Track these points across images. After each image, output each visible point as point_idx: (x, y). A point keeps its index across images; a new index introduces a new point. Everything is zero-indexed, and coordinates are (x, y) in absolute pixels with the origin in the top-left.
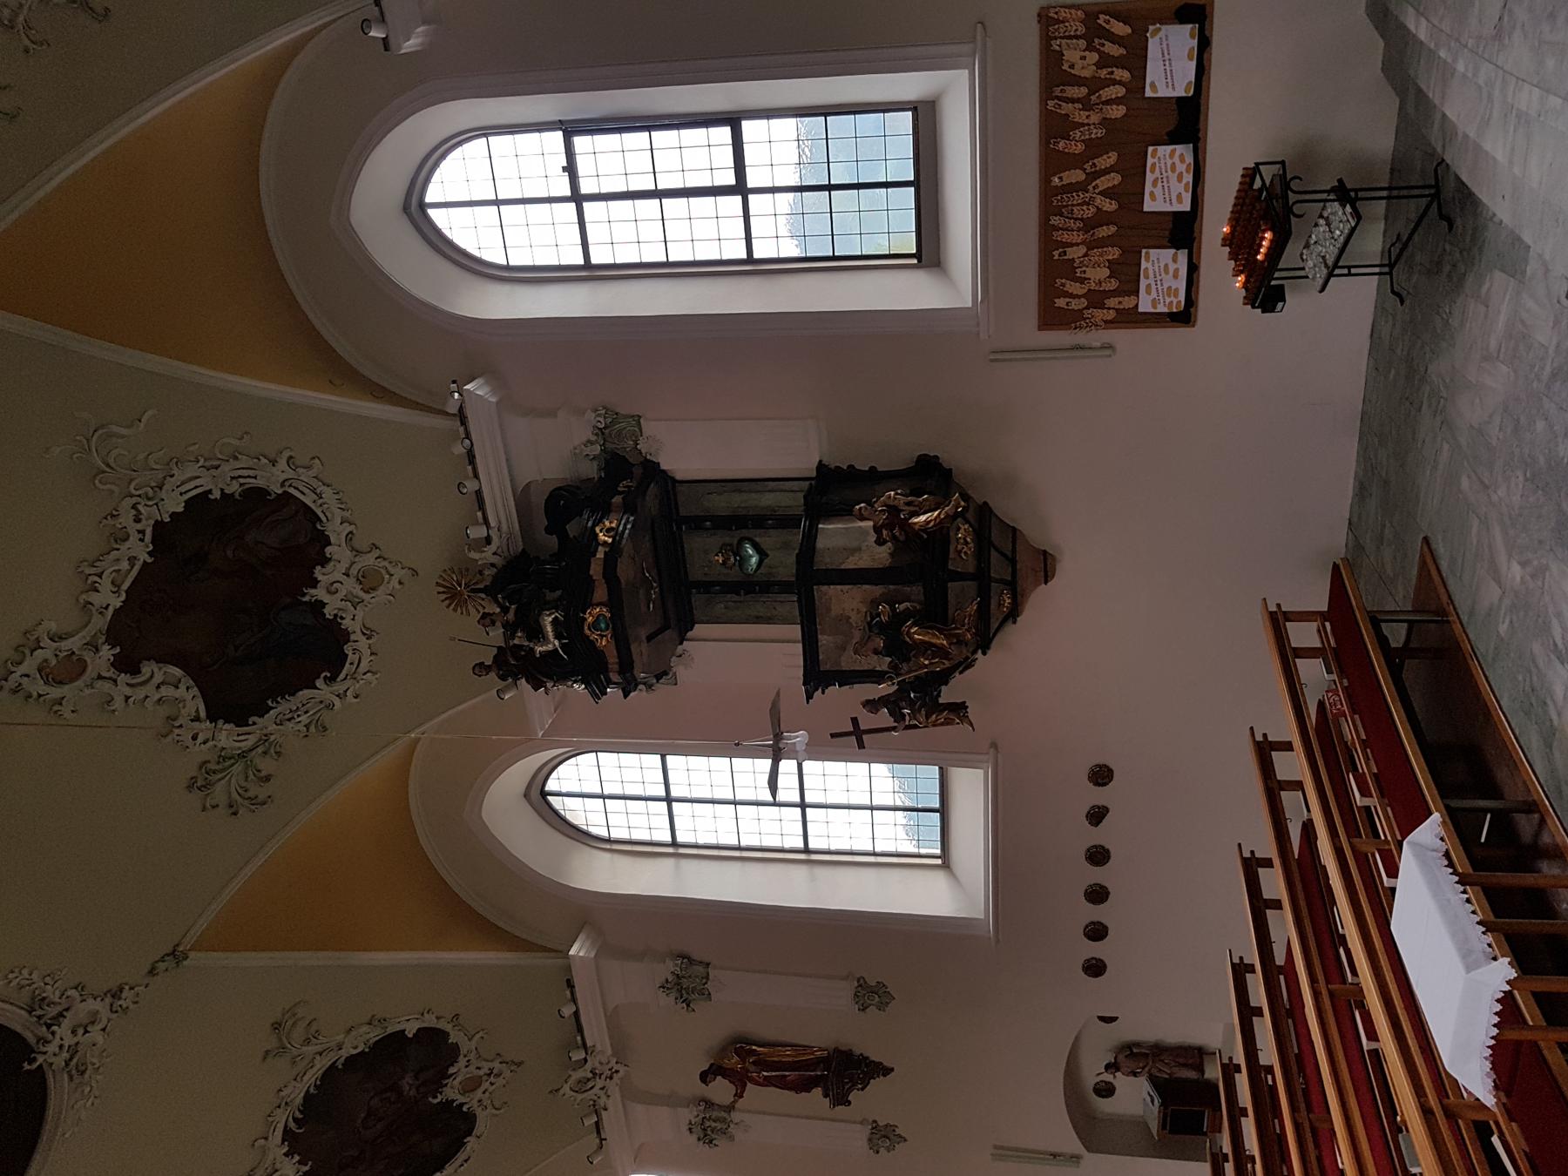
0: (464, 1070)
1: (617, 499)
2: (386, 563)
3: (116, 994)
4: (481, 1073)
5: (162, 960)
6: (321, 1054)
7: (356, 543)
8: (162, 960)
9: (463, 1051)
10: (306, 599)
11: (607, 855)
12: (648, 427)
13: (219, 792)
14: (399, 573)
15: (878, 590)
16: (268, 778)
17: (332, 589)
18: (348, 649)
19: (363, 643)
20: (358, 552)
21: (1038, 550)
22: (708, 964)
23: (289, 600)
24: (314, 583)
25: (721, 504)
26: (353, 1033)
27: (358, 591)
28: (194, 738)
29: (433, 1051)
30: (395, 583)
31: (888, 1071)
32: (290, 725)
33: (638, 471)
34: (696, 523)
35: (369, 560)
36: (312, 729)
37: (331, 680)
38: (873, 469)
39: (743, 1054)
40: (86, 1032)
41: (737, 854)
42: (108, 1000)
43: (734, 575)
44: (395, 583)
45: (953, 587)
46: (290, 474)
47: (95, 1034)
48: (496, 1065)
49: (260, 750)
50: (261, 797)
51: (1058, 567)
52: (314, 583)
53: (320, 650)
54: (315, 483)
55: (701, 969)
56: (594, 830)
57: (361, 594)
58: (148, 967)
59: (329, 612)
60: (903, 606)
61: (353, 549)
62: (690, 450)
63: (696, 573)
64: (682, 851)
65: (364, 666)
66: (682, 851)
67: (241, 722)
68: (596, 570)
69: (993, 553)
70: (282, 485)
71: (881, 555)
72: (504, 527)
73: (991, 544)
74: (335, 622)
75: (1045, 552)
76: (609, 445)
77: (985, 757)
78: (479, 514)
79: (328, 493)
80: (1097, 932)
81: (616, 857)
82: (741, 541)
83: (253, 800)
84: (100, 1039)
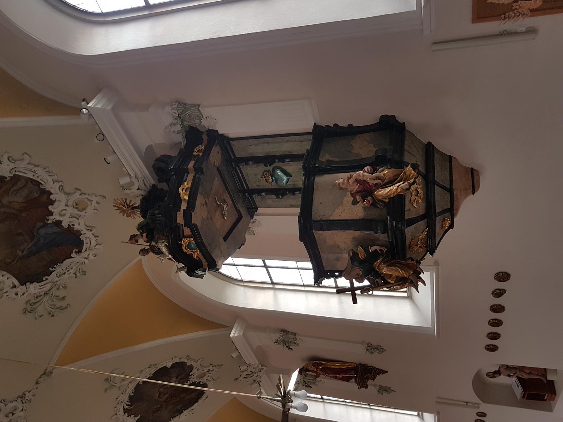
0: (197, 372)
1: (191, 165)
2: (86, 196)
3: (22, 397)
4: (205, 371)
5: (40, 377)
6: (131, 382)
7: (67, 189)
8: (40, 377)
9: (195, 366)
10: (50, 222)
11: (242, 288)
12: (205, 111)
13: (41, 310)
14: (95, 199)
15: (357, 233)
16: (63, 298)
17: (62, 212)
18: (82, 237)
19: (89, 234)
20: (68, 194)
21: (467, 169)
22: (295, 334)
23: (41, 224)
24: (51, 214)
25: (259, 150)
26: (143, 372)
27: (76, 211)
28: (17, 294)
29: (181, 370)
30: (94, 203)
31: (385, 372)
32: (65, 276)
33: (205, 137)
34: (246, 160)
35: (77, 196)
36: (78, 274)
37: (80, 252)
38: (350, 125)
39: (316, 365)
40: (13, 414)
41: (302, 288)
42: (19, 400)
43: (274, 186)
44: (94, 203)
45: (409, 231)
46: (12, 166)
47: (18, 413)
48: (211, 368)
49: (54, 289)
50: (64, 306)
51: (481, 177)
52: (51, 214)
53: (69, 241)
54: (30, 167)
55: (292, 336)
56: (235, 277)
57: (79, 213)
58: (35, 382)
59: (65, 225)
60: (374, 248)
61: (66, 193)
62: (233, 120)
63: (253, 185)
64: (277, 286)
65: (94, 243)
66: (277, 286)
67: (39, 280)
68: (180, 219)
69: (436, 187)
70: (10, 172)
71: (357, 212)
72: (140, 175)
73: (435, 183)
74: (70, 229)
75: (472, 169)
76: (186, 123)
77: (432, 267)
78: (124, 169)
79: (39, 171)
80: (497, 323)
81: (247, 290)
82: (274, 169)
83: (61, 309)
84: (22, 414)
